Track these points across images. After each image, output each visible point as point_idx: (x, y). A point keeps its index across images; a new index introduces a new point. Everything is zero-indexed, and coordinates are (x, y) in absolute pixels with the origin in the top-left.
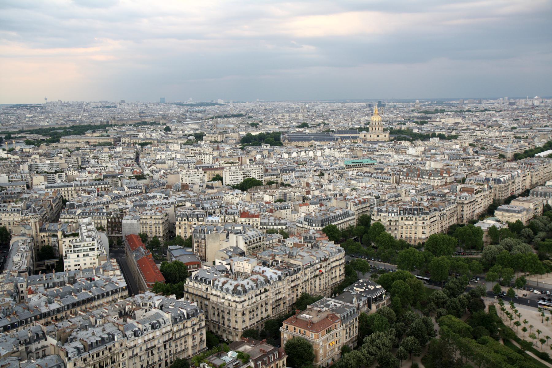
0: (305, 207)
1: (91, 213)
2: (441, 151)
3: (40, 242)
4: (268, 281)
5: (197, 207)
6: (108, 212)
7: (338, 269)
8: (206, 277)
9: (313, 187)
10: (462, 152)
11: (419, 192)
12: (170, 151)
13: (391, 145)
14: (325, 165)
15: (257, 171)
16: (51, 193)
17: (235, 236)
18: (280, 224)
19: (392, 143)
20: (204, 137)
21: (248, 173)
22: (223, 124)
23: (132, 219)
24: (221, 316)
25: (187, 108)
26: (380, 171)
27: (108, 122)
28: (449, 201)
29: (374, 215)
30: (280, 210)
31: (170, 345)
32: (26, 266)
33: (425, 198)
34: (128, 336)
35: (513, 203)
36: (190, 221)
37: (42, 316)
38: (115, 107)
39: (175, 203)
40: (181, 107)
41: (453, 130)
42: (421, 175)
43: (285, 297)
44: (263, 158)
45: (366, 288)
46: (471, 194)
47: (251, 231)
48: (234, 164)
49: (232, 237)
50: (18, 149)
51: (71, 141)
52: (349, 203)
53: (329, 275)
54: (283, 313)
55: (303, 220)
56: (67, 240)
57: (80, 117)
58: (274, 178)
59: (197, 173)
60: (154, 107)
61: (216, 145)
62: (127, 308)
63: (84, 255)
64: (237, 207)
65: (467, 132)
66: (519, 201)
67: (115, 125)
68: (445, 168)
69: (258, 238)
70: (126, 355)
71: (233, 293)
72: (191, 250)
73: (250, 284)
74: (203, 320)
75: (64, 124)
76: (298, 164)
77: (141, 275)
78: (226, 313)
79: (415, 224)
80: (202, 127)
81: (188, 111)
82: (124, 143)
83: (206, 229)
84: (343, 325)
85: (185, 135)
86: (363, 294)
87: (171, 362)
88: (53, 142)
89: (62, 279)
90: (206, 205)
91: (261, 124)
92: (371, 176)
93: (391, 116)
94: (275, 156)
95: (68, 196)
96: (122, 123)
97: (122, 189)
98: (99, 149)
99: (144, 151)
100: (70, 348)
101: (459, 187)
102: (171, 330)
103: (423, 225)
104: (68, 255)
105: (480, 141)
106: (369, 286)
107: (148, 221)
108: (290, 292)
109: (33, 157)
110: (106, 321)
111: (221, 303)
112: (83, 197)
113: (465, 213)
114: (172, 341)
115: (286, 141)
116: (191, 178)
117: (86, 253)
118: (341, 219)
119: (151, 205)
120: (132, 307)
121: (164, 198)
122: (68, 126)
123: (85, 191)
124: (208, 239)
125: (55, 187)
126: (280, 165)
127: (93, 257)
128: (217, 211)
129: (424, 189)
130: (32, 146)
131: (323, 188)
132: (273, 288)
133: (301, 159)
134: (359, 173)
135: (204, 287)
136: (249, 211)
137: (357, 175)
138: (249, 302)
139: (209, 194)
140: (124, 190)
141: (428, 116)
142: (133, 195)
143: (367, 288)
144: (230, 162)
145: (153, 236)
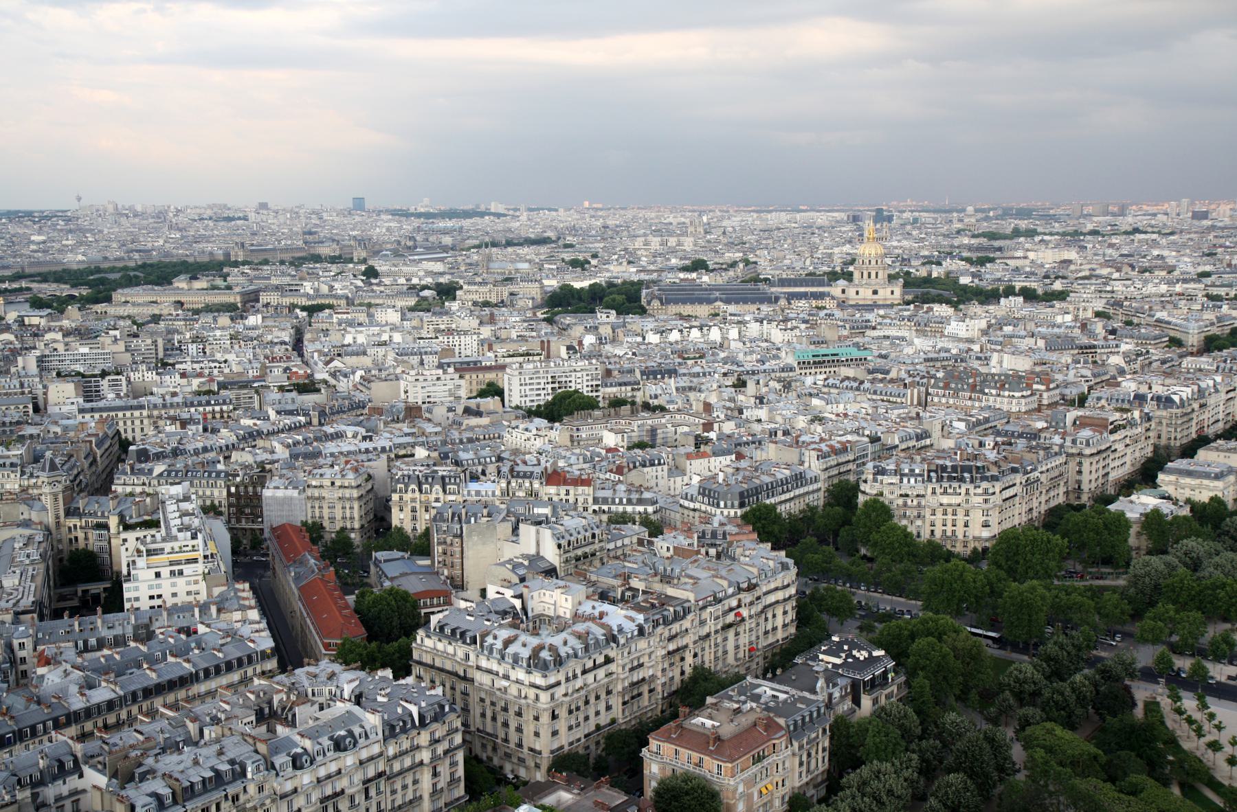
0: (702, 460)
1: (187, 472)
2: (1028, 328)
3: (66, 541)
4: (612, 638)
5: (442, 459)
7: (779, 611)
8: (464, 627)
9: (719, 413)
10: (1077, 332)
11: (974, 426)
12: (377, 325)
13: (906, 313)
14: (750, 362)
15: (585, 374)
16: (93, 424)
17: (533, 529)
18: (640, 502)
19: (909, 310)
20: (459, 293)
21: (563, 379)
22: (503, 260)
23: (286, 488)
24: (500, 719)
25: (416, 222)
26: (880, 376)
27: (227, 255)
28: (1048, 448)
29: (865, 481)
30: (640, 468)
31: (378, 788)
32: (32, 599)
33: (989, 441)
34: (277, 766)
35: (1202, 454)
36: (426, 493)
37: (73, 718)
38: (245, 218)
40: (403, 219)
41: (1057, 278)
42: (979, 384)
43: (653, 677)
44: (601, 343)
45: (847, 657)
46: (1101, 433)
48: (531, 358)
49: (527, 531)
51: (140, 300)
52: (807, 453)
53: (758, 625)
54: (649, 714)
55: (695, 493)
56: (131, 536)
57: (161, 242)
58: (625, 392)
59: (443, 377)
62: (276, 699)
63: (172, 573)
64: (539, 460)
65: (1091, 284)
66: (1217, 449)
68: (1038, 369)
69: (588, 534)
71: (529, 666)
72: (428, 562)
73: (569, 644)
74: (457, 730)
76: (684, 359)
78: (511, 712)
79: (963, 504)
81: (419, 229)
82: (267, 305)
83: (463, 511)
84: (792, 745)
85: (413, 287)
86: (840, 671)
88: (97, 301)
89: (118, 631)
90: (463, 456)
91: (594, 262)
92: (858, 389)
93: (905, 243)
94: (629, 340)
95: (133, 430)
96: (261, 257)
98: (207, 319)
101: (1073, 414)
102: (381, 754)
103: (985, 506)
104: (133, 572)
105: (1121, 306)
106: (855, 652)
107: (325, 493)
108: (666, 665)
109: (49, 336)
110: (227, 732)
111: (500, 689)
112: (169, 435)
113: (1085, 478)
114: (382, 781)
115: (656, 303)
116: (428, 389)
118: (788, 491)
119: (332, 455)
120: (288, 697)
121: (364, 438)
122: (132, 264)
123: (173, 419)
124: (470, 535)
125: (101, 410)
126: (640, 361)
127: (192, 579)
128: (491, 469)
129: (987, 420)
131: (744, 416)
132: (626, 654)
133: (690, 346)
134: (831, 381)
135: (459, 650)
136: (567, 469)
137: (824, 386)
138: (567, 688)
139: (471, 429)
141: (997, 244)
142: (290, 429)
143: (850, 655)
145: (338, 528)
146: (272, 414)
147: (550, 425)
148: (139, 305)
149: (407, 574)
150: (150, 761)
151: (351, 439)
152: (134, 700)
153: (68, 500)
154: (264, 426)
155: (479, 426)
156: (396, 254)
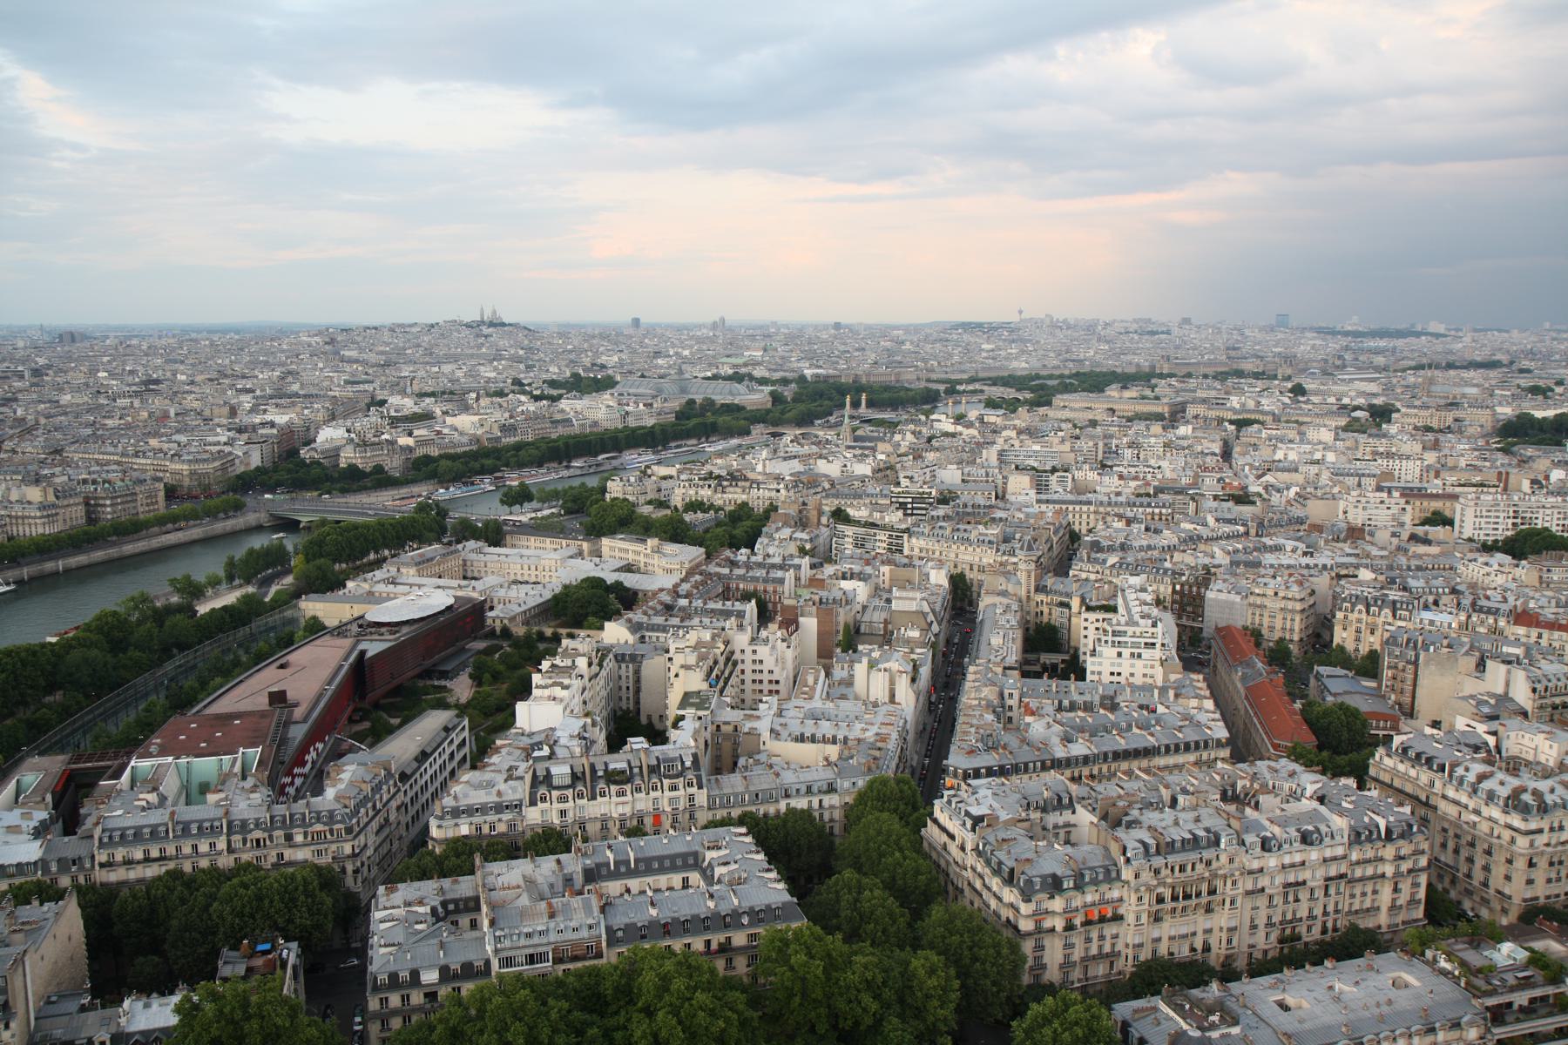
3: (1033, 614)
5: (1389, 583)
6: (1177, 568)
8: (1431, 753)
12: (1309, 443)
15: (1556, 511)
17: (1503, 668)
20: (1394, 415)
21: (1528, 515)
22: (1447, 384)
24: (1464, 853)
25: (1344, 341)
27: (1153, 367)
31: (1338, 888)
32: (1014, 658)
34: (1247, 844)
36: (1374, 615)
37: (1057, 764)
38: (1168, 333)
39: (1332, 568)
40: (1329, 337)
47: (1552, 662)
48: (1485, 489)
49: (1496, 671)
50: (973, 415)
51: (1077, 405)
56: (1092, 616)
57: (1092, 353)
59: (1387, 501)
60: (1259, 336)
61: (1430, 436)
63: (1132, 655)
67: (1171, 375)
70: (1240, 884)
71: (1506, 805)
72: (1373, 684)
74: (1423, 852)
75: (1059, 367)
77: (1255, 720)
80: (1388, 389)
81: (1347, 348)
82: (1196, 417)
83: (1420, 639)
85: (1344, 407)
87: (1335, 930)
88: (1040, 405)
89: (1087, 698)
90: (1412, 583)
91: (1559, 390)
96: (1184, 371)
97: (1201, 521)
98: (1139, 426)
99: (1243, 440)
100: (1131, 838)
102: (1344, 857)
104: (1098, 649)
107: (1267, 602)
109: (1005, 433)
110: (1201, 802)
111: (1467, 823)
112: (1117, 530)
114: (1343, 882)
116: (1369, 512)
117: (1136, 651)
119: (1272, 566)
120: (1252, 785)
121: (1305, 554)
122: (1067, 372)
123: (1120, 517)
124: (1427, 663)
125: (1055, 502)
128: (1444, 600)
130: (1001, 412)
135: (1424, 776)
138: (1550, 838)
139: (1420, 557)
140: (1205, 524)
142: (1228, 537)
144: (1474, 481)
145: (1276, 638)
146: (1211, 520)
147: (1515, 562)
148: (1075, 410)
149: (1351, 693)
150: (1135, 813)
151: (1290, 553)
152: (1105, 760)
153: (1039, 578)
154: (1204, 532)
155: (1429, 555)
156: (1325, 373)
